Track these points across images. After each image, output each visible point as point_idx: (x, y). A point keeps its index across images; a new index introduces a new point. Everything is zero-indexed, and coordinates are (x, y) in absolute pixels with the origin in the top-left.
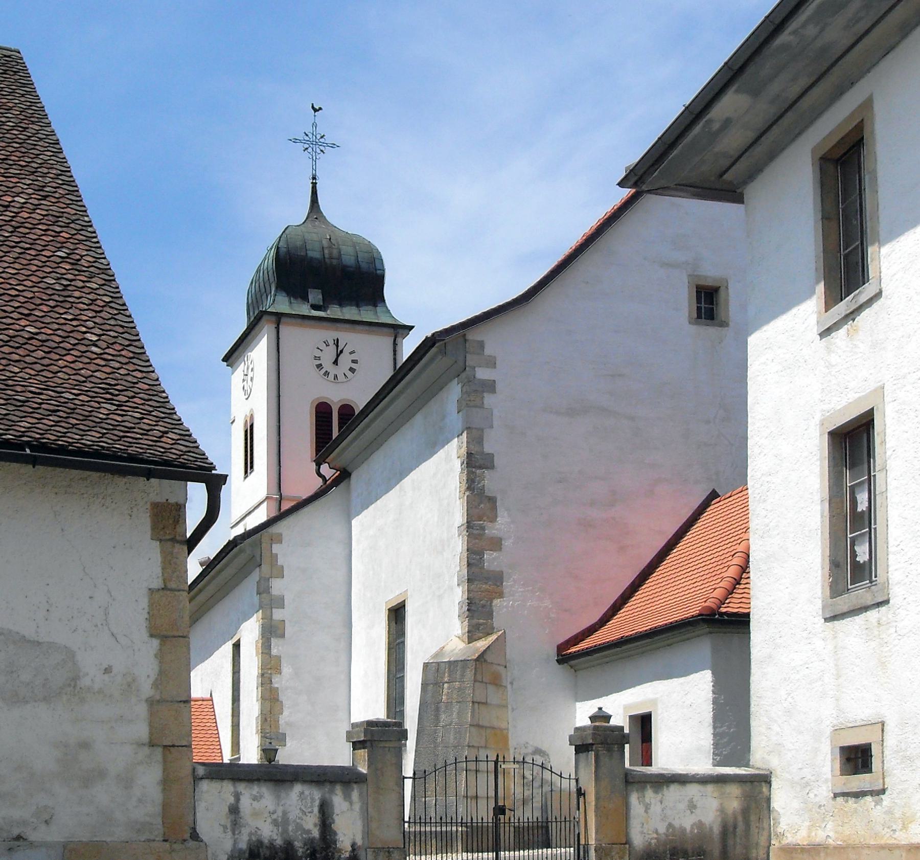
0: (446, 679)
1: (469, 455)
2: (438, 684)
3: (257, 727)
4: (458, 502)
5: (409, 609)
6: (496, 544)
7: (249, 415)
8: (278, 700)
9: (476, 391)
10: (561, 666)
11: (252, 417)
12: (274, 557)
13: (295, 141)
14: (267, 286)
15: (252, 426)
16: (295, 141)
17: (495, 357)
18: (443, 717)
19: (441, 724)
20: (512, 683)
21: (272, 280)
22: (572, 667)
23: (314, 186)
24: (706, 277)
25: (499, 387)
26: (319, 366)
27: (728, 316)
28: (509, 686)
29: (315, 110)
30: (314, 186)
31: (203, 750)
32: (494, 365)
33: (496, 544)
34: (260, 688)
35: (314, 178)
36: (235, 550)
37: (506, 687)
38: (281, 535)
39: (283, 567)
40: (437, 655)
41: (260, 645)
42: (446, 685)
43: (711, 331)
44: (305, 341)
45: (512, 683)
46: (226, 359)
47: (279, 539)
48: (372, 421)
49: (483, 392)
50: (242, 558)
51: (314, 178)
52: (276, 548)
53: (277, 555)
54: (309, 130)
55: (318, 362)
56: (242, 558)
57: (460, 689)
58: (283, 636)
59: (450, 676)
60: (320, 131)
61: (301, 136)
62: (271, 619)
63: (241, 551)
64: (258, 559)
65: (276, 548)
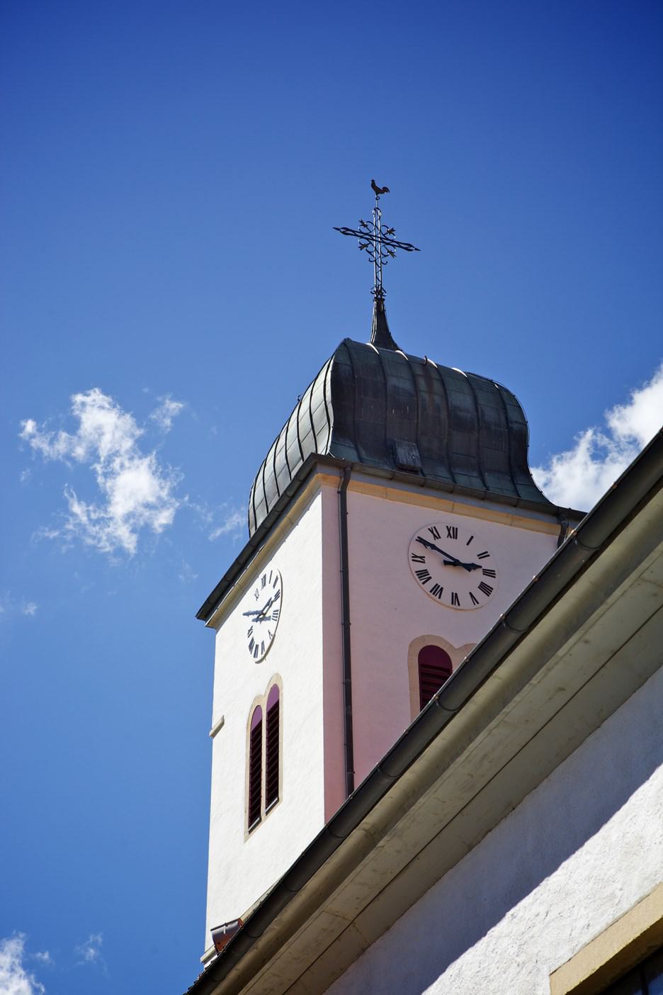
16: (346, 231)
23: (380, 302)
26: (423, 575)
29: (378, 191)
30: (380, 302)
46: (205, 613)
55: (421, 567)
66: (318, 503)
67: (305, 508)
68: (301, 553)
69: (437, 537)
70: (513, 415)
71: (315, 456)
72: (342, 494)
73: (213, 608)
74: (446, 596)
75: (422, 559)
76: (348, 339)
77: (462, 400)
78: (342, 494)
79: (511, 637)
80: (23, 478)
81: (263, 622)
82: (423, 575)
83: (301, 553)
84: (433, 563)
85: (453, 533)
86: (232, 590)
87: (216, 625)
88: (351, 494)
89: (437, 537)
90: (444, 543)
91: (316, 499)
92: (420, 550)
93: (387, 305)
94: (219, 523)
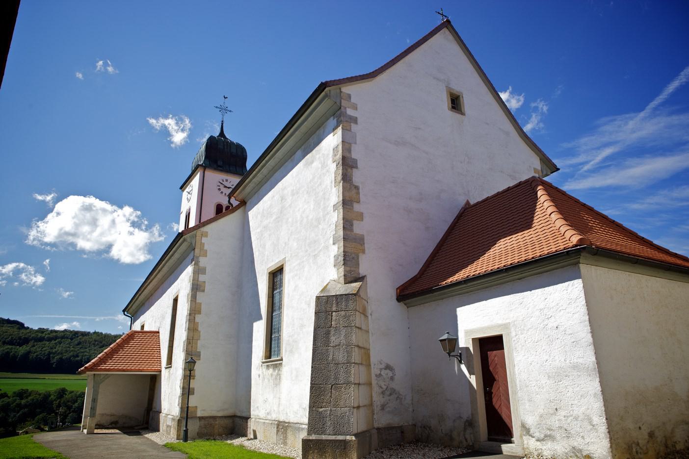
0: (334, 309)
1: (344, 158)
2: (329, 313)
3: (184, 347)
4: (334, 189)
5: (286, 269)
6: (360, 217)
7: (188, 208)
8: (198, 330)
9: (347, 121)
10: (399, 304)
11: (190, 209)
12: (202, 245)
13: (217, 107)
14: (201, 157)
15: (189, 213)
16: (217, 107)
17: (357, 105)
18: (333, 338)
19: (332, 345)
20: (371, 315)
21: (203, 154)
22: (405, 304)
23: (222, 124)
24: (453, 89)
25: (359, 121)
26: (219, 189)
27: (464, 111)
28: (370, 317)
29: (225, 98)
30: (222, 124)
31: (443, 255)
32: (356, 109)
33: (360, 217)
34: (188, 323)
35: (222, 122)
36: (182, 239)
37: (368, 317)
38: (207, 232)
39: (207, 251)
40: (323, 290)
41: (190, 296)
42: (334, 314)
43: (457, 116)
44: (215, 177)
45: (371, 315)
46: (181, 188)
47: (205, 235)
48: (267, 162)
49: (351, 122)
50: (184, 247)
51: (222, 122)
52: (204, 240)
53: (204, 244)
54: (222, 104)
55: (219, 188)
56: (184, 247)
57: (345, 317)
58: (203, 291)
59: (337, 306)
60: (226, 105)
61: (219, 106)
62: (198, 281)
63: (185, 240)
64: (194, 245)
65: (204, 240)
66: (199, 173)
67: (195, 176)
68: (196, 182)
69: (223, 181)
70: (244, 154)
71: (198, 165)
72: (204, 172)
73: (183, 187)
74: (224, 194)
75: (219, 186)
76: (212, 136)
77: (234, 150)
78: (204, 172)
79: (170, 250)
80: (119, 327)
81: (94, 331)
82: (219, 189)
83: (196, 182)
84: (222, 187)
85: (227, 181)
86: (187, 183)
87: (183, 191)
88: (206, 172)
89: (223, 181)
90: (225, 183)
91: (195, 178)
92: (219, 184)
93: (224, 125)
94: (60, 417)
